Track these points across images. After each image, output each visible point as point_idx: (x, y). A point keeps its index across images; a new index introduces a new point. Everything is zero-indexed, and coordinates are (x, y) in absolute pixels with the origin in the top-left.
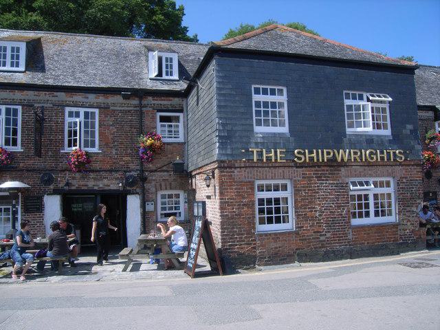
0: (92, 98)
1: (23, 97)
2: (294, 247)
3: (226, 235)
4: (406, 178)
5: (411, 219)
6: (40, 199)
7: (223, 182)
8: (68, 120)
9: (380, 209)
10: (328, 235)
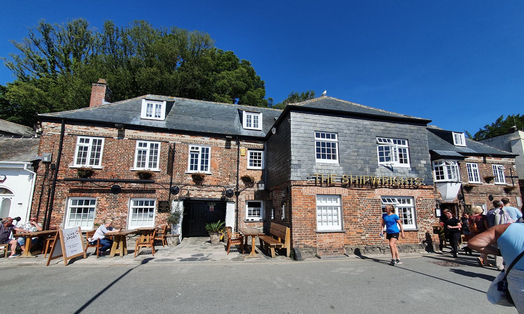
10: (367, 235)
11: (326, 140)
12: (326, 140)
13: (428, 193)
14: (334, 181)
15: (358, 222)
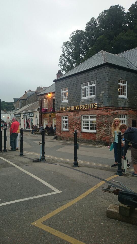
4: (100, 115)
5: (101, 132)
7: (100, 187)
9: (122, 92)
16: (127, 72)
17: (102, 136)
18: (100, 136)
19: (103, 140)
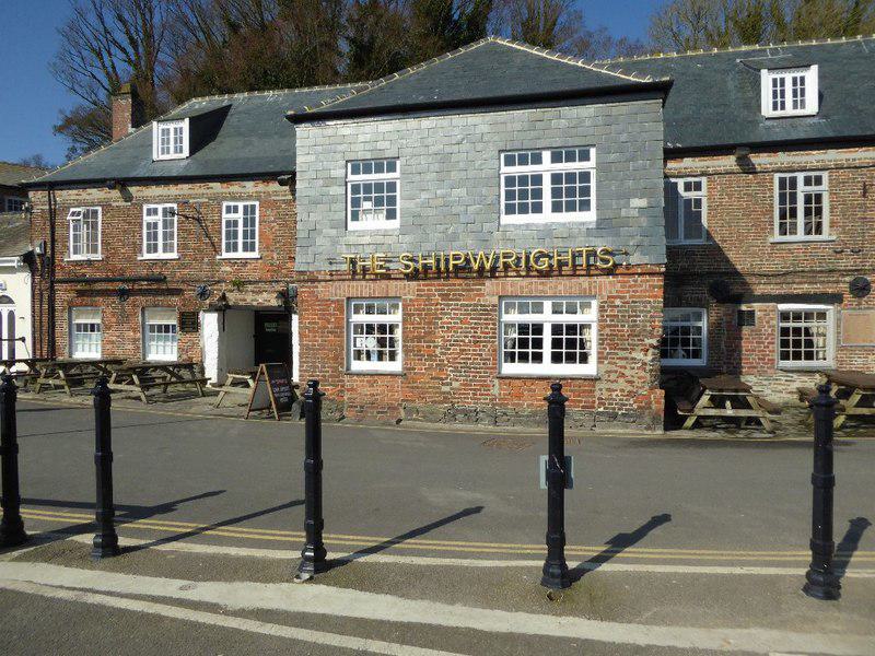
0: (250, 186)
1: (178, 192)
2: (399, 396)
3: (305, 371)
6: (195, 315)
8: (147, 219)
10: (456, 385)
11: (373, 177)
12: (373, 177)
13: (646, 286)
14: (397, 267)
15: (436, 356)
16: (814, 152)
17: (630, 388)
18: (622, 390)
19: (635, 406)
